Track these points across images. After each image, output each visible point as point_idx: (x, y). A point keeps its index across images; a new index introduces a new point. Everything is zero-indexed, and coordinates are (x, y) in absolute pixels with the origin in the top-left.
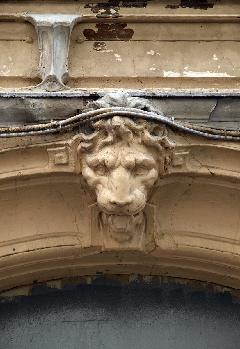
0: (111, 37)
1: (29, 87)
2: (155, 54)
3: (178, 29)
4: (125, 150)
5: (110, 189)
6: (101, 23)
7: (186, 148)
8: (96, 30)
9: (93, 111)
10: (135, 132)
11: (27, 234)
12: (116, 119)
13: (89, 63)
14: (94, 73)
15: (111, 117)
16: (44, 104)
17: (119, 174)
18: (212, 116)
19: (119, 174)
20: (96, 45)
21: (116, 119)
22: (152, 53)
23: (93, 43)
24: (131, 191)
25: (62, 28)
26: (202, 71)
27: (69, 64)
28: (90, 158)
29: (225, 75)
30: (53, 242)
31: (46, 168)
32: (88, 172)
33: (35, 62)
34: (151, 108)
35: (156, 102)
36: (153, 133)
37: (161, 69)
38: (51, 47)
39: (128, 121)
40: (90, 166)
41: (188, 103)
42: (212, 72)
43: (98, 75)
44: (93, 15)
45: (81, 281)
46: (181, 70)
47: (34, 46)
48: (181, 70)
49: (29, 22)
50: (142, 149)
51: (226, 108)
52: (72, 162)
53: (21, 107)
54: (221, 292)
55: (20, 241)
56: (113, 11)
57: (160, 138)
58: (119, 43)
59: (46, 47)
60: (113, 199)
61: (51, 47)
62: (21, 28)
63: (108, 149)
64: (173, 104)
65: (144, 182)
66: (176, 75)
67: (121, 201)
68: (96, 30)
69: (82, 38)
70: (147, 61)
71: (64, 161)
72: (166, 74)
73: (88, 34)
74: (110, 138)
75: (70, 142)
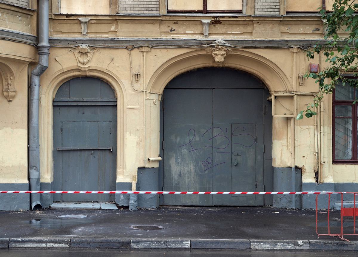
0: (217, 24)
1: (201, 36)
2: (226, 28)
3: (231, 22)
4: (221, 52)
5: (218, 59)
6: (215, 21)
7: (232, 50)
8: (214, 22)
9: (215, 44)
10: (223, 48)
11: (200, 63)
12: (219, 46)
13: (213, 30)
14: (214, 32)
15: (218, 46)
16: (205, 41)
17: (219, 56)
18: (237, 44)
19: (219, 56)
20: (214, 25)
21: (219, 46)
22: (225, 27)
23: (213, 25)
24: (221, 59)
25: (208, 23)
26: (235, 32)
27: (209, 31)
28: (214, 53)
29: (240, 33)
30: (206, 64)
31: (205, 53)
32: (213, 55)
33: (202, 30)
34: (226, 43)
35: (227, 41)
36: (226, 48)
37: (227, 31)
38: (206, 28)
39: (222, 46)
40: (214, 54)
41: (233, 41)
42: (237, 32)
43: (215, 32)
44: (214, 19)
45: (329, 204)
46: (231, 31)
47: (202, 26)
48: (231, 31)
49: (201, 21)
50: (224, 51)
51: (240, 42)
52: (210, 52)
53: (201, 42)
54: (308, 178)
55: (198, 65)
56: (218, 18)
57: (227, 49)
58: (219, 25)
59: (204, 27)
60: (218, 61)
61: (206, 28)
62: (199, 22)
63: (218, 51)
64: (230, 42)
65: (224, 57)
66: (230, 33)
67: (220, 61)
68: (214, 22)
69: (211, 24)
70: (224, 29)
71: (209, 52)
72: (228, 32)
73: (213, 23)
74: (218, 49)
75: (210, 49)
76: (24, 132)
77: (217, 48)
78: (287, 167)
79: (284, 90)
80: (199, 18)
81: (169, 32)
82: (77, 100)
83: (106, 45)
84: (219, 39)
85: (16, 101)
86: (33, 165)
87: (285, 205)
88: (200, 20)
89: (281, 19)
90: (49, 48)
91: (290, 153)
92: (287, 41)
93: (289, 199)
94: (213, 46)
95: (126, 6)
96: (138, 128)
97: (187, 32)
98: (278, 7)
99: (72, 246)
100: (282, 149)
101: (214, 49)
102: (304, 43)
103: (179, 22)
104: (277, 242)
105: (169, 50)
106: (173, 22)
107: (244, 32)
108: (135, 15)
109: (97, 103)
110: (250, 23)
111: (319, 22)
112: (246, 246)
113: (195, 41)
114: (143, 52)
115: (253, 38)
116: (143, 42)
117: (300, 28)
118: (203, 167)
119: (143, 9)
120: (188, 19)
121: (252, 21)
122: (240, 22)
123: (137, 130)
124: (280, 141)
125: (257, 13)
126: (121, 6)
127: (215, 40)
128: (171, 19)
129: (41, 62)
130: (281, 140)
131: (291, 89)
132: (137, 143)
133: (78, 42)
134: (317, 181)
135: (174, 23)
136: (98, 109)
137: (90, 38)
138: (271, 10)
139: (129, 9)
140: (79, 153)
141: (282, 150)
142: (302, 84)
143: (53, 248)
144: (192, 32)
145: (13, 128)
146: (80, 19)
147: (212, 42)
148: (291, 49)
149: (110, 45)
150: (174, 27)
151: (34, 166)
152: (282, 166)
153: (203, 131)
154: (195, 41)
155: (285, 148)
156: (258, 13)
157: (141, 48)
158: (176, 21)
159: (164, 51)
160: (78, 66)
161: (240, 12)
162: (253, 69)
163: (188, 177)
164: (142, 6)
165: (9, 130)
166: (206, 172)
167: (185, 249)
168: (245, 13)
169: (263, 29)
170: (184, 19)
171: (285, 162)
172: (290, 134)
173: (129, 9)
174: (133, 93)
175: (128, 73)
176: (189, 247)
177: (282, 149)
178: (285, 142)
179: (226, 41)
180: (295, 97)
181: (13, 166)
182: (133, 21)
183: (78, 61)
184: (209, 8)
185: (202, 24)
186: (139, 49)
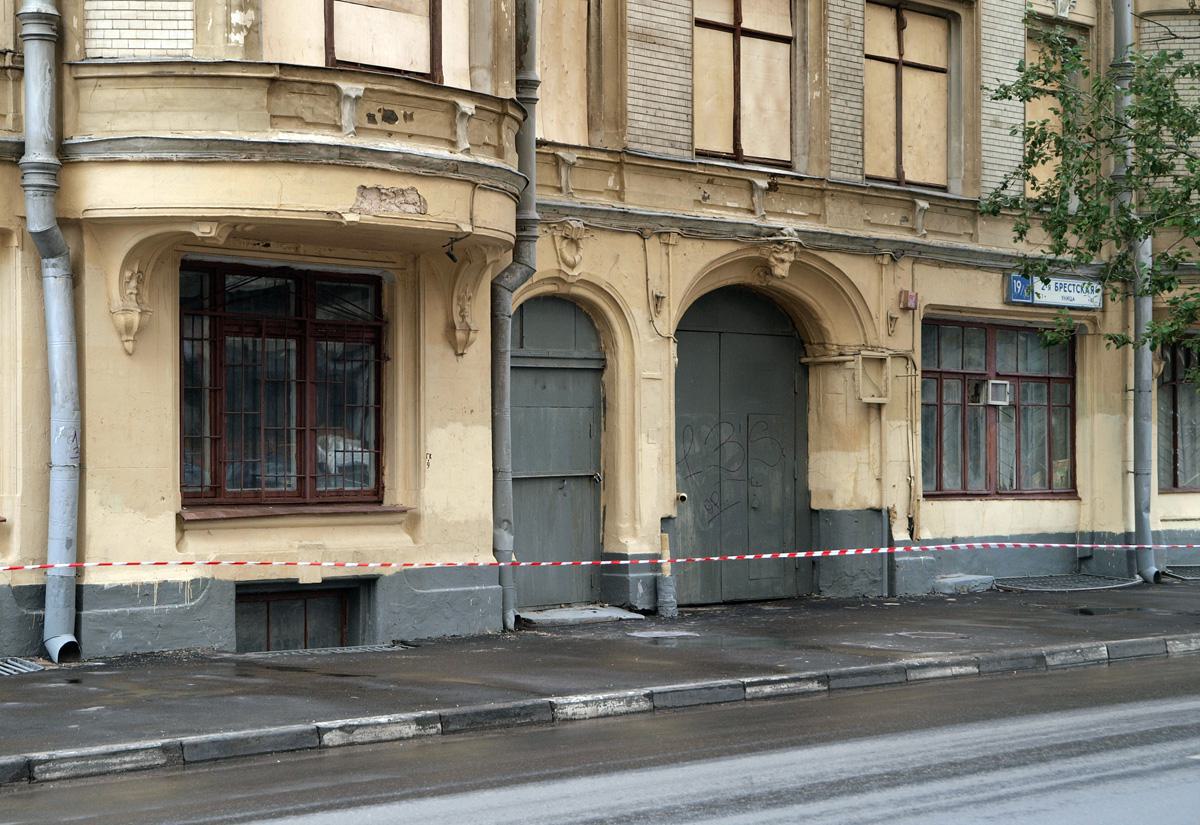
3: (792, 189)
31: (757, 254)
70: (781, 204)
74: (787, 250)
76: (486, 433)
77: (786, 247)
78: (868, 509)
79: (857, 343)
80: (748, 174)
81: (700, 201)
82: (538, 354)
83: (608, 222)
84: (789, 226)
85: (471, 352)
86: (504, 518)
87: (864, 590)
88: (749, 178)
89: (865, 192)
90: (58, 170)
91: (875, 481)
92: (877, 240)
93: (871, 577)
94: (779, 242)
95: (638, 132)
96: (660, 425)
97: (729, 204)
98: (860, 165)
99: (983, 668)
100: (857, 470)
101: (781, 248)
102: (901, 246)
103: (717, 180)
104: (1190, 638)
105: (707, 243)
106: (707, 178)
107: (811, 214)
108: (653, 156)
109: (570, 361)
110: (819, 193)
111: (909, 204)
112: (1159, 649)
113: (750, 228)
114: (668, 244)
115: (827, 228)
116: (669, 222)
117: (883, 214)
118: (706, 513)
119: (667, 143)
120: (732, 174)
121: (823, 190)
122: (805, 190)
123: (659, 429)
124: (852, 454)
125: (833, 174)
126: (631, 130)
127: (782, 229)
128: (707, 172)
129: (527, 260)
130: (854, 450)
131: (875, 343)
132: (659, 459)
133: (561, 211)
134: (911, 535)
135: (709, 182)
136: (570, 376)
137: (582, 203)
138: (851, 170)
139: (643, 140)
140: (538, 484)
141: (857, 472)
142: (893, 332)
143: (961, 676)
144: (736, 205)
145: (466, 425)
146: (561, 153)
147: (775, 231)
148: (879, 258)
149: (615, 224)
150: (709, 189)
151: (504, 521)
152: (856, 506)
153: (705, 429)
154: (750, 228)
155: (864, 468)
156: (835, 175)
157: (665, 236)
158: (711, 178)
159: (698, 244)
160: (560, 271)
161: (787, 165)
162: (807, 294)
163: (683, 539)
164: (666, 136)
165: (458, 427)
166: (711, 525)
167: (1098, 662)
168: (801, 169)
169: (838, 210)
170: (725, 173)
171: (866, 498)
172: (874, 439)
173: (643, 140)
174: (652, 340)
175: (641, 292)
176: (1106, 656)
177: (857, 470)
178: (863, 455)
179: (798, 231)
180: (889, 359)
181: (466, 522)
182: (649, 169)
183: (562, 258)
184: (908, 177)
185: (752, 186)
186: (659, 238)
